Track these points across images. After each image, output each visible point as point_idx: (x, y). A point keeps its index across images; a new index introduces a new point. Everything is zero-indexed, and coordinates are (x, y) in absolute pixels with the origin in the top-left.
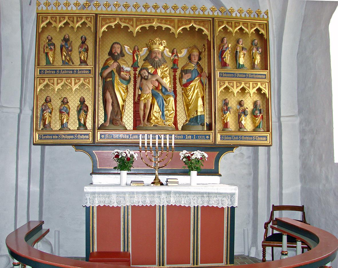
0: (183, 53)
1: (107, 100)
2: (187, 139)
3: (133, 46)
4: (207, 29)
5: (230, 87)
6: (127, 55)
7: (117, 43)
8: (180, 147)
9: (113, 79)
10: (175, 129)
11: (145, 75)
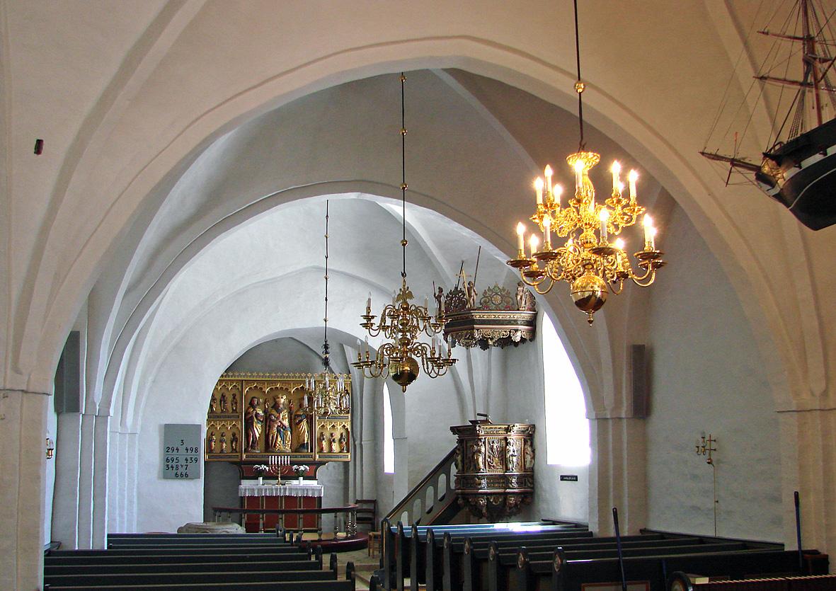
8: (293, 463)
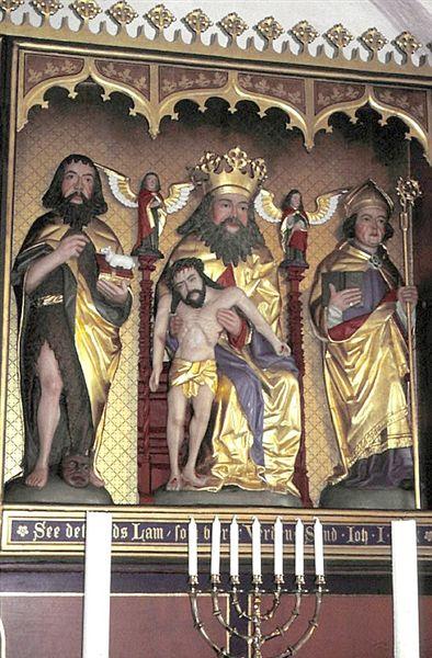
0: (325, 213)
1: (42, 380)
2: (351, 544)
3: (141, 174)
4: (422, 121)
6: (116, 207)
7: (77, 158)
9: (70, 299)
10: (299, 501)
11: (191, 288)
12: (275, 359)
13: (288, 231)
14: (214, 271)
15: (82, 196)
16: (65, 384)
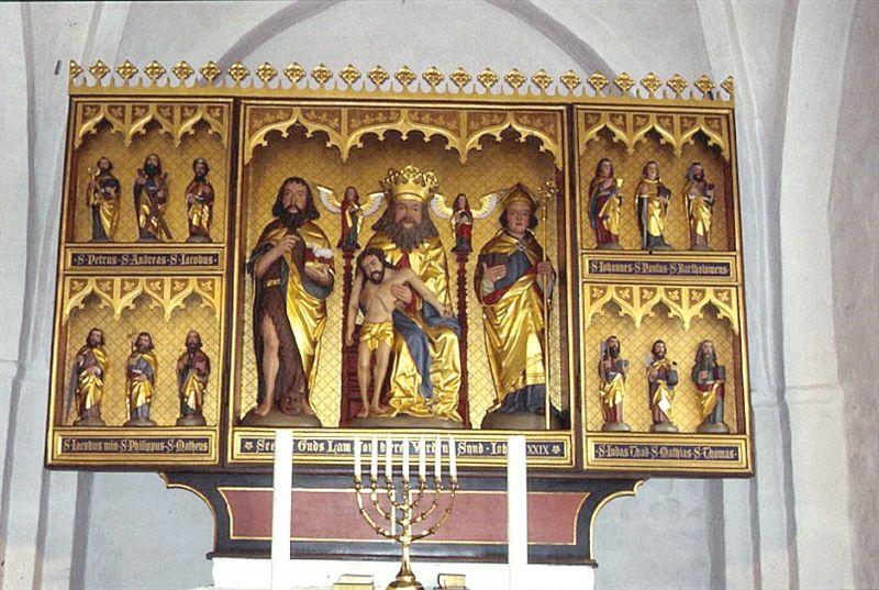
5: (670, 303)
6: (326, 213)
12: (439, 321)
13: (457, 224)
14: (394, 256)
15: (297, 207)
16: (281, 342)
